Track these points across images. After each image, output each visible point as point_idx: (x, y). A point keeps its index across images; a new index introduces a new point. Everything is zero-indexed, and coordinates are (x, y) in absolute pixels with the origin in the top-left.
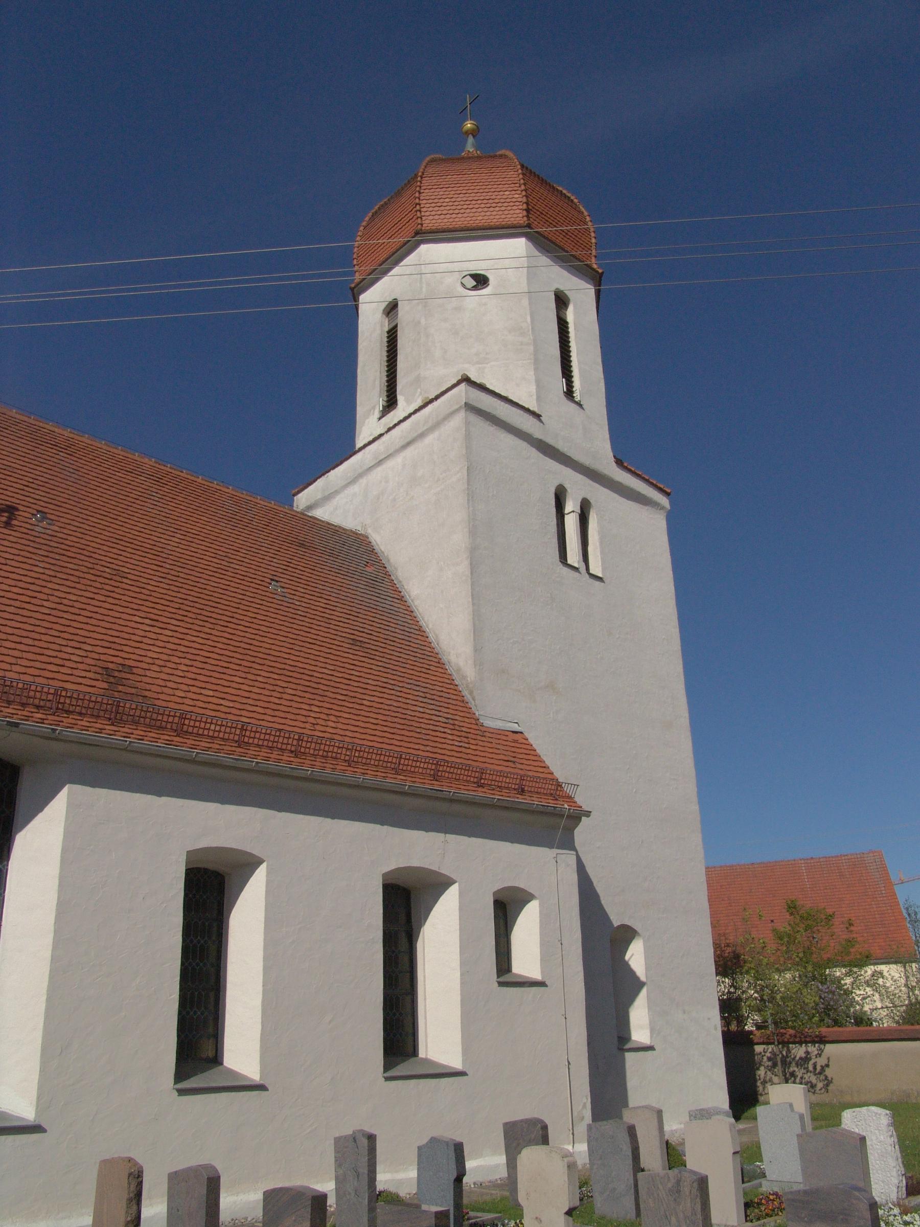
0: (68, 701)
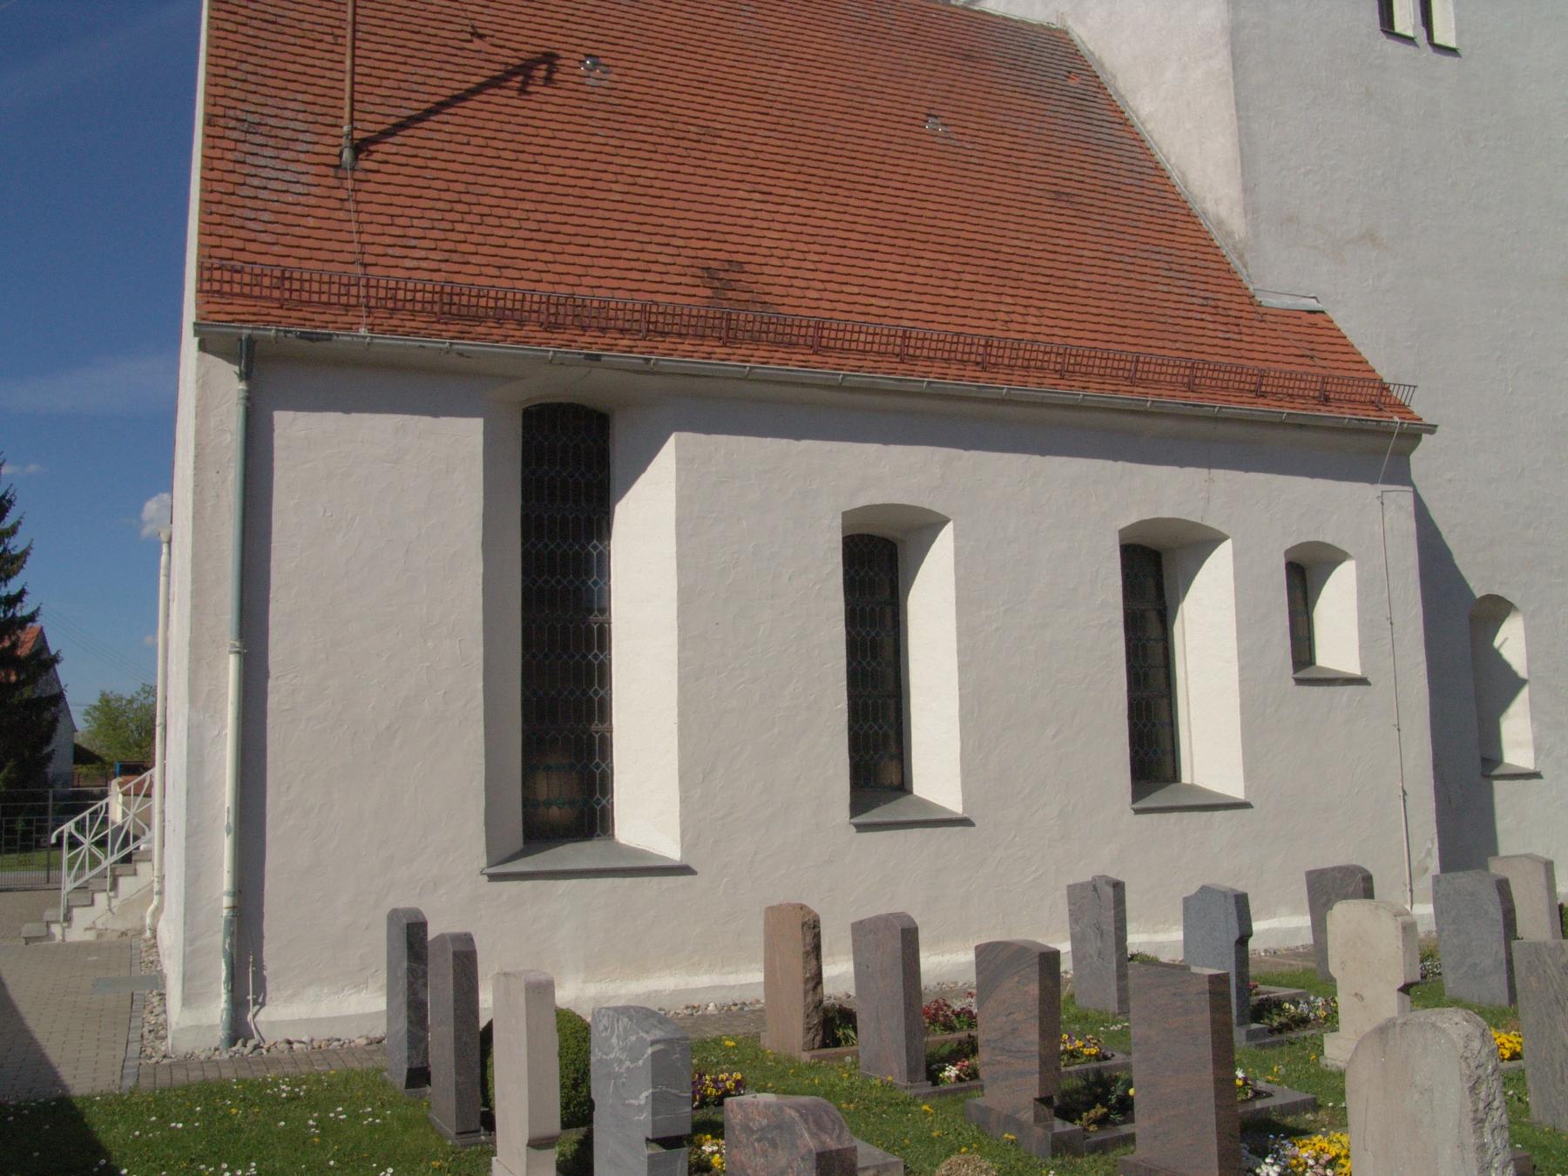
0: (661, 319)
